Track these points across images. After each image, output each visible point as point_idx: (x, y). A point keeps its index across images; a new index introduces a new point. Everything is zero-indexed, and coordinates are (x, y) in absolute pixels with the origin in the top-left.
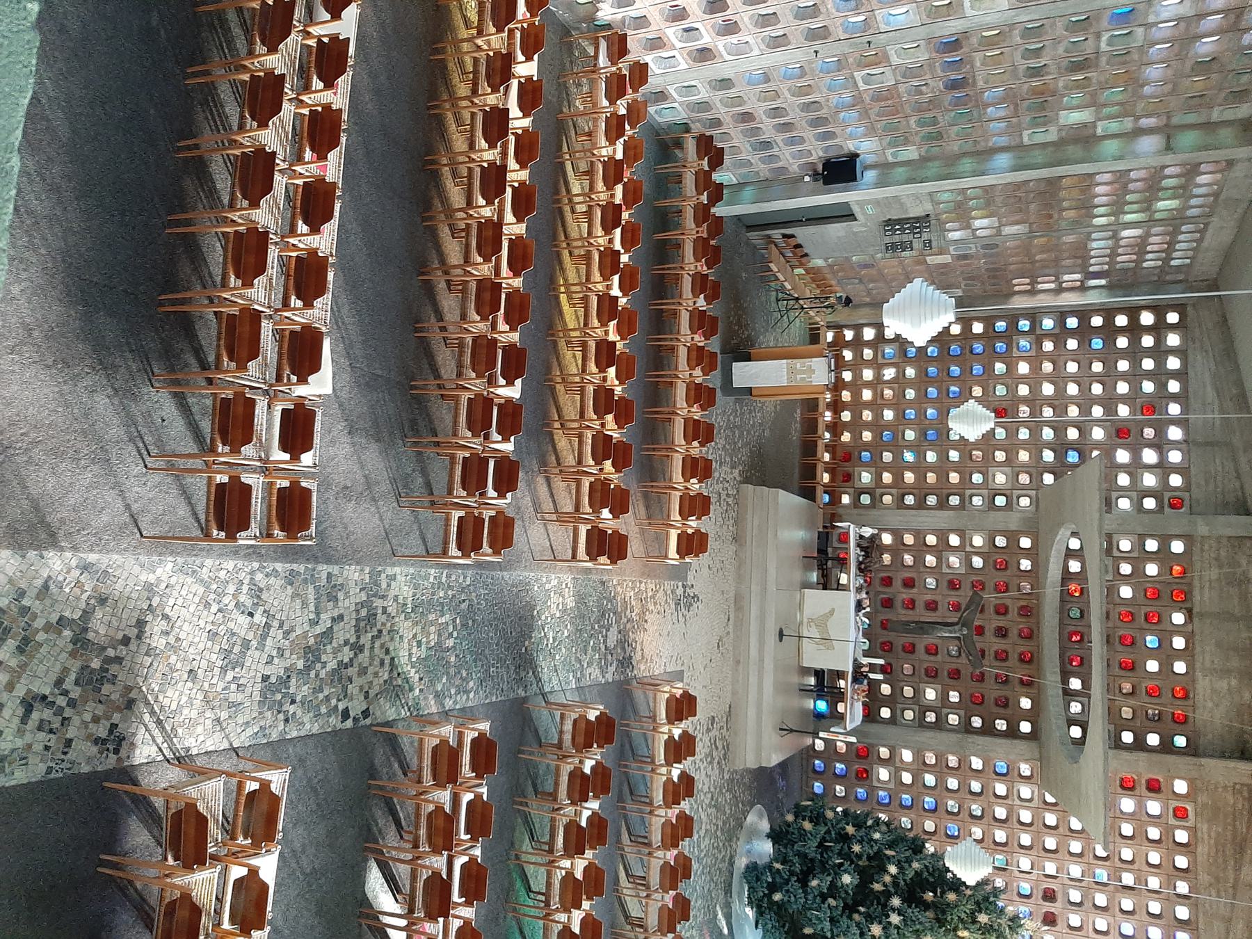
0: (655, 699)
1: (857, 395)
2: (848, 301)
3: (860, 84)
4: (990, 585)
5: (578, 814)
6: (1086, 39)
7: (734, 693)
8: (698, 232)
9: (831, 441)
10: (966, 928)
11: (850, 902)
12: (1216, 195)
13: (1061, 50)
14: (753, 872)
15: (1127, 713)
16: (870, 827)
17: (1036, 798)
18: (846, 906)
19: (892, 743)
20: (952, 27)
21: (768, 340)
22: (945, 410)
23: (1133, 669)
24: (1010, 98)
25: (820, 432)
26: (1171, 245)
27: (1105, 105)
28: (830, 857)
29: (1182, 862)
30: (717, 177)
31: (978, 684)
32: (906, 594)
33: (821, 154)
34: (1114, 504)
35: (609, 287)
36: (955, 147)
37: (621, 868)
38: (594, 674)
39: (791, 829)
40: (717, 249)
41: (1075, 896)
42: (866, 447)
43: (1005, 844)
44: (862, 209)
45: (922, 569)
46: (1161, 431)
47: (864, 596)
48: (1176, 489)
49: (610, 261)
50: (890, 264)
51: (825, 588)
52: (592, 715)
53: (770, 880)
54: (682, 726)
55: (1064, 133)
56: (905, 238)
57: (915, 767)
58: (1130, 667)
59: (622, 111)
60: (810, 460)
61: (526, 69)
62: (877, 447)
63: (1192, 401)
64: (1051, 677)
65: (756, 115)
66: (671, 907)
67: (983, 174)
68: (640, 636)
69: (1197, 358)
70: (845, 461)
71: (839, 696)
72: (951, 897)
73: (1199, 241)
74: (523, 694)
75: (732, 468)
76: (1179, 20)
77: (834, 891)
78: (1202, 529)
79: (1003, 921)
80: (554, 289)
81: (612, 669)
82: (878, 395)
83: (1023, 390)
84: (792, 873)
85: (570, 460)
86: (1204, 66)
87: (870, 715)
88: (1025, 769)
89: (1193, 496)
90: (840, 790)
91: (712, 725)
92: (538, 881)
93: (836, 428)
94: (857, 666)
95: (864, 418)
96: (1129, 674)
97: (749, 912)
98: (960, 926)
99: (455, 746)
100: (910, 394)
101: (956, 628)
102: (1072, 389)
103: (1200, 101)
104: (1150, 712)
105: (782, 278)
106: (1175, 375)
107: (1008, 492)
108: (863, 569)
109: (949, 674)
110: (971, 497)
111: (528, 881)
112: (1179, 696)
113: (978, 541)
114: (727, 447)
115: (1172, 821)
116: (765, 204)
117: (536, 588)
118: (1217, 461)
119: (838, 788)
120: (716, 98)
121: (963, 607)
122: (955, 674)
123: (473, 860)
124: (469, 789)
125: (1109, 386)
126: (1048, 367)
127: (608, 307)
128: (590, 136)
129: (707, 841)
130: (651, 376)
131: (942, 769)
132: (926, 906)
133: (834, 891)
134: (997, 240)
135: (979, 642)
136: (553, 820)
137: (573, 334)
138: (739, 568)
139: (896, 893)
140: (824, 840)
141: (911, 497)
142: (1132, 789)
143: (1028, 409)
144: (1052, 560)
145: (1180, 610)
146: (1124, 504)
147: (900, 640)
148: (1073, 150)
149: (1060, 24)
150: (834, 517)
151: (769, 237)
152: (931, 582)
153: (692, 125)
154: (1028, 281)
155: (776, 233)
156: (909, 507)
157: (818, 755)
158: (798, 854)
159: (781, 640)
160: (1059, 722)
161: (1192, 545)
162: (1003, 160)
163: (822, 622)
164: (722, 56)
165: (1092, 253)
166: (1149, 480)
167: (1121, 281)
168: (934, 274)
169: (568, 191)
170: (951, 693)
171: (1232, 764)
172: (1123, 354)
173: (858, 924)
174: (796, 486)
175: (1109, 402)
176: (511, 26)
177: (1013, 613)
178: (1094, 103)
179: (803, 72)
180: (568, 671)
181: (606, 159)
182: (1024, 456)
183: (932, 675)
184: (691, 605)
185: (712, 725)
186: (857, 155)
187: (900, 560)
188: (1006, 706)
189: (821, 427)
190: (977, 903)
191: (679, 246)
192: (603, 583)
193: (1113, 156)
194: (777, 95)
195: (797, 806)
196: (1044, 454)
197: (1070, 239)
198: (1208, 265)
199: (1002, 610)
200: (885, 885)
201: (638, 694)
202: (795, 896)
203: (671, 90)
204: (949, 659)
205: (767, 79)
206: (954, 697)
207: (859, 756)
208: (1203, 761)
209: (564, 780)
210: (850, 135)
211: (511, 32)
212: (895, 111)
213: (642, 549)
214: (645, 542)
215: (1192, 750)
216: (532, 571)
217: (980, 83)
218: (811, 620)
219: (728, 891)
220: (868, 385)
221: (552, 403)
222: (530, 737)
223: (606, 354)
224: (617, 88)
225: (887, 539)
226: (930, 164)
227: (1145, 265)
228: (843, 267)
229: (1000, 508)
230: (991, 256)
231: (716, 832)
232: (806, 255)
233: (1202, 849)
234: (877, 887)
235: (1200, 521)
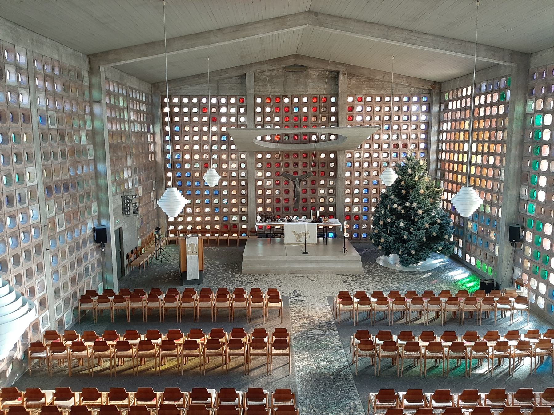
0: (343, 310)
1: (199, 223)
2: (158, 229)
3: (63, 229)
4: (277, 169)
5: (401, 345)
6: (51, 134)
7: (332, 273)
8: (128, 300)
9: (219, 234)
10: (414, 177)
11: (410, 222)
12: (118, 84)
13: (55, 144)
14: (404, 262)
15: (324, 119)
16: (379, 215)
17: (359, 152)
18: (412, 224)
19: (343, 206)
20: (41, 190)
21: (175, 263)
22: (205, 187)
23: (307, 117)
24: (74, 165)
25: (215, 238)
26: (138, 101)
27: (80, 126)
28: (394, 231)
29: (378, 99)
30: (100, 292)
31: (317, 173)
32: (283, 202)
33: (92, 244)
34: (243, 123)
35: (158, 345)
36: (93, 187)
37: (415, 322)
38: (336, 340)
39: (384, 247)
40: (136, 291)
41: (395, 137)
42: (221, 219)
43: (378, 163)
44: (117, 225)
45: (272, 195)
46: (214, 106)
47: (285, 218)
48: (236, 100)
49: (145, 346)
50: (142, 211)
51: (284, 234)
52: (357, 341)
53: (406, 255)
54: (352, 297)
55: (90, 143)
56: (131, 206)
57: (352, 197)
58: (306, 118)
59: (70, 343)
60: (228, 242)
61: (49, 396)
62: (221, 214)
63: (200, 94)
64: (313, 146)
65: (73, 276)
66: (429, 299)
67: (106, 175)
68: (316, 319)
69: (183, 92)
70: (227, 227)
71: (326, 228)
72: (403, 183)
73: (136, 90)
74: (351, 376)
75: (235, 277)
76: (46, 98)
77: (407, 229)
78: (252, 91)
79: (410, 163)
80: (158, 373)
81: (333, 332)
82: (198, 214)
83: (197, 157)
84: (403, 246)
85: (241, 359)
86: (65, 88)
87: (333, 215)
88: (348, 156)
90: (364, 227)
91: (347, 283)
92: (431, 363)
93: (213, 232)
96: (309, 118)
97: (420, 263)
98: (414, 179)
99: (386, 411)
100: (198, 201)
102: (196, 138)
103: (81, 90)
104: (323, 110)
105: (147, 259)
106: (190, 100)
107: (239, 163)
108: (274, 220)
109: (313, 185)
110: (242, 177)
111: (432, 367)
112: (316, 100)
113: (259, 174)
114: (225, 280)
115: (363, 102)
116: (114, 268)
117: (303, 373)
119: (363, 227)
120: (63, 295)
121: (287, 179)
122: (314, 182)
123: (433, 397)
124: (402, 402)
125: (195, 125)
126: (187, 147)
127: (167, 345)
128: (80, 359)
129: (396, 283)
130: (196, 320)
131: (352, 187)
132: (408, 192)
133: (407, 229)
134: (133, 168)
135: (300, 173)
136: (405, 357)
137: (180, 361)
139: (404, 204)
140: (387, 233)
141: (242, 200)
142: (352, 117)
143: (205, 155)
144: (267, 146)
145: (283, 100)
146: (243, 119)
147: (302, 204)
148: (98, 139)
149: (43, 145)
150: (253, 232)
151: (127, 266)
152: (277, 192)
153: (75, 306)
154: (150, 155)
155: (126, 262)
156: (247, 201)
157: (351, 236)
158: (394, 244)
159: (308, 253)
161: (258, 95)
162: (100, 167)
163: (298, 236)
164: (44, 294)
165: (140, 130)
166: (233, 110)
167: (151, 119)
168: (146, 192)
169: (108, 368)
170: (321, 184)
171: (340, 82)
172: (181, 119)
173: (419, 219)
174: (241, 248)
175: (201, 124)
176: (25, 406)
177: (288, 160)
178: (78, 131)
179: (56, 255)
180: (337, 353)
182: (224, 157)
183: (314, 191)
184: (298, 294)
185: (347, 283)
186: (94, 228)
187: (269, 204)
188: (324, 163)
189: (213, 238)
190: (404, 173)
191: (133, 309)
192: (295, 338)
193: (102, 123)
194: (65, 266)
195: (374, 245)
197: (134, 139)
198: (146, 87)
199: (287, 165)
200: (402, 209)
201: (342, 318)
202: (412, 245)
203: (58, 318)
204: (308, 185)
205: (57, 272)
206: (322, 182)
207: (350, 220)
208: (340, 92)
209: (387, 353)
210: (85, 232)
211: (28, 407)
212: (76, 213)
213: (277, 320)
214: (273, 318)
215: (337, 95)
216: (295, 376)
217: (67, 177)
218: (298, 240)
219: (413, 273)
220: (194, 219)
221: (213, 371)
222: (370, 371)
223: (190, 345)
224: (58, 347)
225: (260, 210)
226: (100, 197)
227: (145, 110)
228: (141, 232)
229: (246, 166)
230: (139, 169)
231: (391, 279)
232: (136, 248)
233: (373, 92)
234: (403, 212)
235: (248, 92)
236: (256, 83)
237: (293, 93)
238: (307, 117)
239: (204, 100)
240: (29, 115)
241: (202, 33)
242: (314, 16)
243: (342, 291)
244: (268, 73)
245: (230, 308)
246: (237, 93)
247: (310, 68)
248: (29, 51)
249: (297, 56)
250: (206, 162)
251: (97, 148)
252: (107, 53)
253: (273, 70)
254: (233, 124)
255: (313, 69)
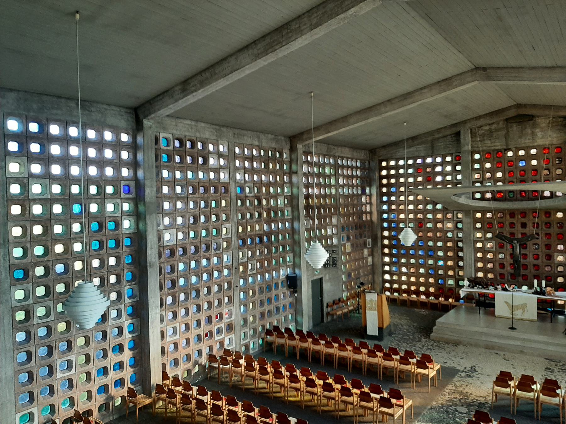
7: (539, 356)
22: (419, 247)
33: (285, 289)
42: (436, 281)
48: (452, 159)
58: (535, 170)
60: (409, 303)
62: (437, 277)
63: (527, 145)
69: (399, 155)
89: (454, 152)
93: (427, 294)
94: (536, 293)
95: (423, 281)
101: (514, 245)
104: (557, 162)
113: (479, 235)
118: (440, 144)
122: (548, 247)
126: (402, 207)
138: (471, 345)
146: (459, 177)
148: (295, 203)
152: (501, 256)
155: (325, 310)
159: (515, 329)
160: (557, 201)
161: (476, 151)
162: (296, 225)
166: (449, 168)
167: (366, 181)
172: (397, 180)
181: (359, 399)
183: (550, 257)
196: (438, 208)
198: (362, 155)
204: (540, 249)
226: (295, 250)
236: (473, 139)
237: (518, 146)
238: (536, 170)
239: (419, 161)
240: (228, 188)
241: (374, 106)
242: (482, 72)
243: (502, 370)
244: (487, 128)
245: (535, 402)
246: (453, 151)
247: (538, 116)
248: (231, 142)
249: (519, 106)
250: (420, 222)
251: (294, 209)
252: (302, 134)
253: (493, 123)
254: (449, 182)
255: (542, 117)
